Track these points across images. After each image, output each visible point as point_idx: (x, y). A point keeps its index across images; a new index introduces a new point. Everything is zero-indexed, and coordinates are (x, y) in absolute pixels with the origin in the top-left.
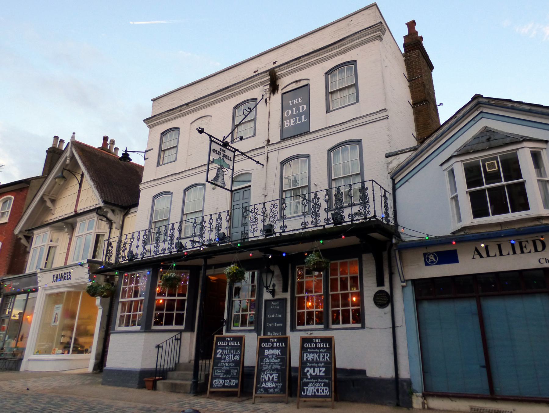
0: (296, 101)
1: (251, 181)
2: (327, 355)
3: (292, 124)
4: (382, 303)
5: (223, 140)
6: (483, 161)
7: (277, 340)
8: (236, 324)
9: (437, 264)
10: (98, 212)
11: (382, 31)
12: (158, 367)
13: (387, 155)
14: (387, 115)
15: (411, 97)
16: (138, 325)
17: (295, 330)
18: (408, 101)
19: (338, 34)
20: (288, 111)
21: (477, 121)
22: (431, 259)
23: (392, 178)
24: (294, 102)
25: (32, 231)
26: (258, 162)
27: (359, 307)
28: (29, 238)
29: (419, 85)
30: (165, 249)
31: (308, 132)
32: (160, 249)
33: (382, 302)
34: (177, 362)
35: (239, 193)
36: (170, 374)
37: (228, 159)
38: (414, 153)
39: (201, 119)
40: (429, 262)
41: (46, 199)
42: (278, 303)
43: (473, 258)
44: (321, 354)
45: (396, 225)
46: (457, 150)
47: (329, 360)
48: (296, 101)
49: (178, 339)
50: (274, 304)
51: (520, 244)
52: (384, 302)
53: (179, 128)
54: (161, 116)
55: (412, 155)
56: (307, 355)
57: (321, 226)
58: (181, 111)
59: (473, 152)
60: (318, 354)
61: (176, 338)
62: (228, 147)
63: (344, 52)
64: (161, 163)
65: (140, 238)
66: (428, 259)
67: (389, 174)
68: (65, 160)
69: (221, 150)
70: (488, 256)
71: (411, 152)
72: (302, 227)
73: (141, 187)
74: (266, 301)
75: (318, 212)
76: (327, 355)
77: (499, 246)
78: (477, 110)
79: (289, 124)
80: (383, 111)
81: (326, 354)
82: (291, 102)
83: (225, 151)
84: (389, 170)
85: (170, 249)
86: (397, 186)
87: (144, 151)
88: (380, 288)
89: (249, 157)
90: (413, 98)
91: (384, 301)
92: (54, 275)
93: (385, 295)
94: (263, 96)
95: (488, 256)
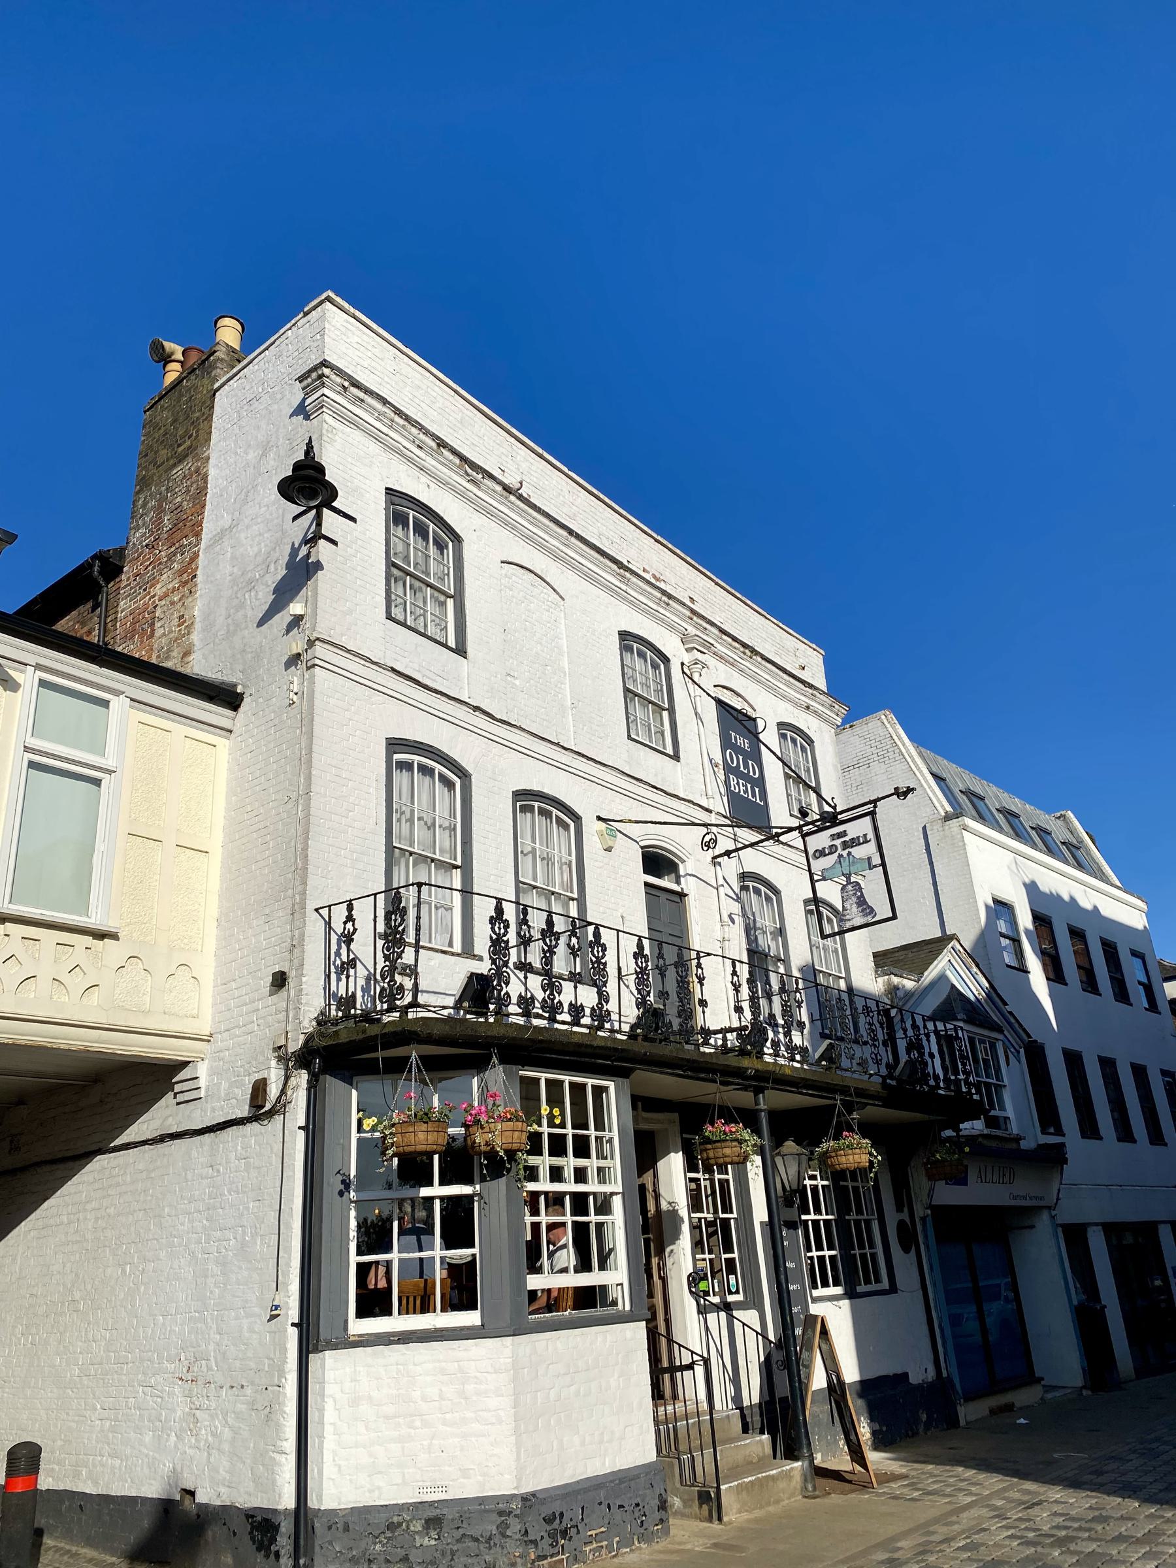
87: (893, 791)
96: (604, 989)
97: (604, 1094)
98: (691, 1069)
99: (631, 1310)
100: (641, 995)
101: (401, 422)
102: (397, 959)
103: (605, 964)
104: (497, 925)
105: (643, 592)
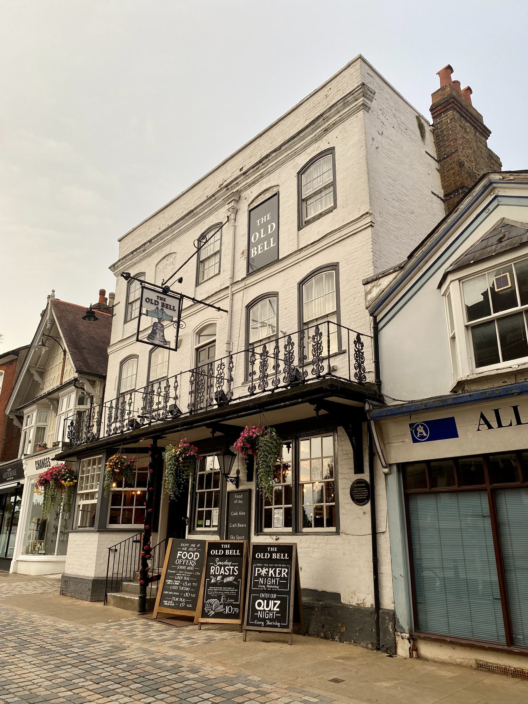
0: (264, 220)
1: (215, 335)
2: (285, 571)
3: (259, 252)
4: (360, 498)
5: (162, 285)
7: (230, 546)
8: (200, 522)
9: (429, 440)
10: (76, 385)
11: (368, 96)
12: (110, 574)
13: (365, 283)
14: (371, 222)
15: (442, 185)
17: (261, 533)
18: (432, 193)
20: (256, 234)
21: (490, 211)
22: (420, 433)
23: (371, 315)
24: (262, 220)
25: (22, 410)
26: (219, 308)
27: (333, 504)
28: (21, 418)
29: (454, 164)
31: (278, 261)
32: (112, 428)
33: (361, 497)
35: (204, 351)
37: (170, 309)
38: (400, 275)
39: (167, 258)
40: (418, 437)
41: (33, 371)
42: (241, 496)
43: (479, 430)
44: (277, 569)
45: (379, 382)
46: (453, 263)
47: (286, 576)
48: (264, 220)
50: (238, 497)
52: (363, 497)
53: (145, 273)
54: (126, 260)
55: (397, 278)
56: (259, 570)
57: (270, 390)
58: (144, 250)
59: (474, 262)
60: (274, 569)
61: (135, 539)
62: (169, 293)
63: (319, 138)
64: (129, 319)
66: (416, 432)
67: (367, 308)
68: (46, 324)
69: (158, 299)
70: (500, 425)
71: (397, 273)
72: (249, 393)
73: (109, 350)
74: (229, 493)
75: (292, 364)
76: (285, 571)
77: (515, 409)
78: (489, 194)
79: (256, 252)
80: (365, 216)
81: (283, 569)
82: (258, 221)
83: (165, 300)
84: (367, 303)
86: (381, 325)
88: (359, 476)
90: (444, 187)
91: (363, 494)
92: (36, 462)
93: (363, 487)
94: (228, 217)
95: (500, 425)
96: (362, 365)
101: (124, 260)
102: (319, 355)
103: (363, 353)
104: (358, 345)
105: (204, 209)
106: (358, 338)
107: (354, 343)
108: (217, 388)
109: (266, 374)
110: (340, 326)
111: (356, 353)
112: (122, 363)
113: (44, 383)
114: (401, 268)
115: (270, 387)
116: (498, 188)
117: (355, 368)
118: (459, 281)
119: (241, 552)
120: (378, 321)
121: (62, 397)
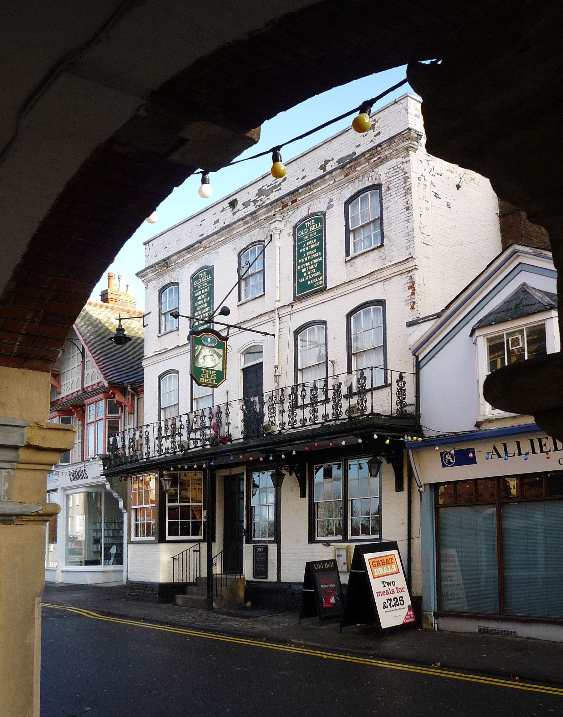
6: (507, 334)
16: (152, 536)
19: (177, 235)
22: (448, 460)
26: (266, 332)
30: (305, 420)
34: (198, 576)
36: (190, 588)
40: (446, 463)
49: (196, 551)
51: (540, 440)
65: (197, 420)
66: (445, 459)
73: (144, 363)
75: (340, 402)
77: (518, 443)
85: (337, 416)
89: (246, 329)
96: (404, 401)
97: (530, 420)
98: (347, 432)
99: (196, 582)
100: (400, 399)
104: (400, 383)
106: (401, 377)
107: (397, 382)
108: (270, 418)
109: (316, 409)
110: (384, 369)
111: (398, 391)
112: (161, 377)
113: (60, 386)
114: (438, 316)
115: (320, 420)
116: (521, 256)
117: (397, 405)
118: (484, 336)
119: (298, 262)
120: (419, 360)
121: (88, 405)
